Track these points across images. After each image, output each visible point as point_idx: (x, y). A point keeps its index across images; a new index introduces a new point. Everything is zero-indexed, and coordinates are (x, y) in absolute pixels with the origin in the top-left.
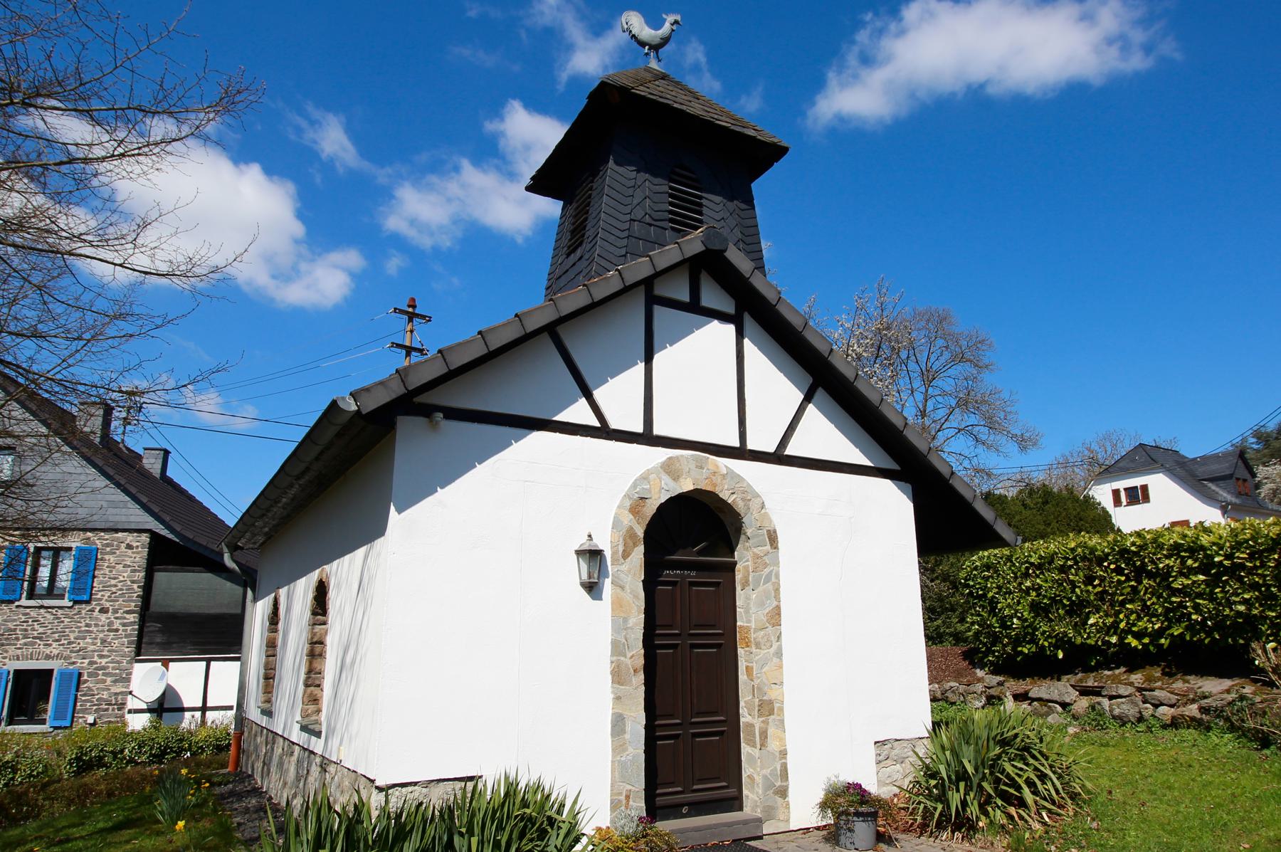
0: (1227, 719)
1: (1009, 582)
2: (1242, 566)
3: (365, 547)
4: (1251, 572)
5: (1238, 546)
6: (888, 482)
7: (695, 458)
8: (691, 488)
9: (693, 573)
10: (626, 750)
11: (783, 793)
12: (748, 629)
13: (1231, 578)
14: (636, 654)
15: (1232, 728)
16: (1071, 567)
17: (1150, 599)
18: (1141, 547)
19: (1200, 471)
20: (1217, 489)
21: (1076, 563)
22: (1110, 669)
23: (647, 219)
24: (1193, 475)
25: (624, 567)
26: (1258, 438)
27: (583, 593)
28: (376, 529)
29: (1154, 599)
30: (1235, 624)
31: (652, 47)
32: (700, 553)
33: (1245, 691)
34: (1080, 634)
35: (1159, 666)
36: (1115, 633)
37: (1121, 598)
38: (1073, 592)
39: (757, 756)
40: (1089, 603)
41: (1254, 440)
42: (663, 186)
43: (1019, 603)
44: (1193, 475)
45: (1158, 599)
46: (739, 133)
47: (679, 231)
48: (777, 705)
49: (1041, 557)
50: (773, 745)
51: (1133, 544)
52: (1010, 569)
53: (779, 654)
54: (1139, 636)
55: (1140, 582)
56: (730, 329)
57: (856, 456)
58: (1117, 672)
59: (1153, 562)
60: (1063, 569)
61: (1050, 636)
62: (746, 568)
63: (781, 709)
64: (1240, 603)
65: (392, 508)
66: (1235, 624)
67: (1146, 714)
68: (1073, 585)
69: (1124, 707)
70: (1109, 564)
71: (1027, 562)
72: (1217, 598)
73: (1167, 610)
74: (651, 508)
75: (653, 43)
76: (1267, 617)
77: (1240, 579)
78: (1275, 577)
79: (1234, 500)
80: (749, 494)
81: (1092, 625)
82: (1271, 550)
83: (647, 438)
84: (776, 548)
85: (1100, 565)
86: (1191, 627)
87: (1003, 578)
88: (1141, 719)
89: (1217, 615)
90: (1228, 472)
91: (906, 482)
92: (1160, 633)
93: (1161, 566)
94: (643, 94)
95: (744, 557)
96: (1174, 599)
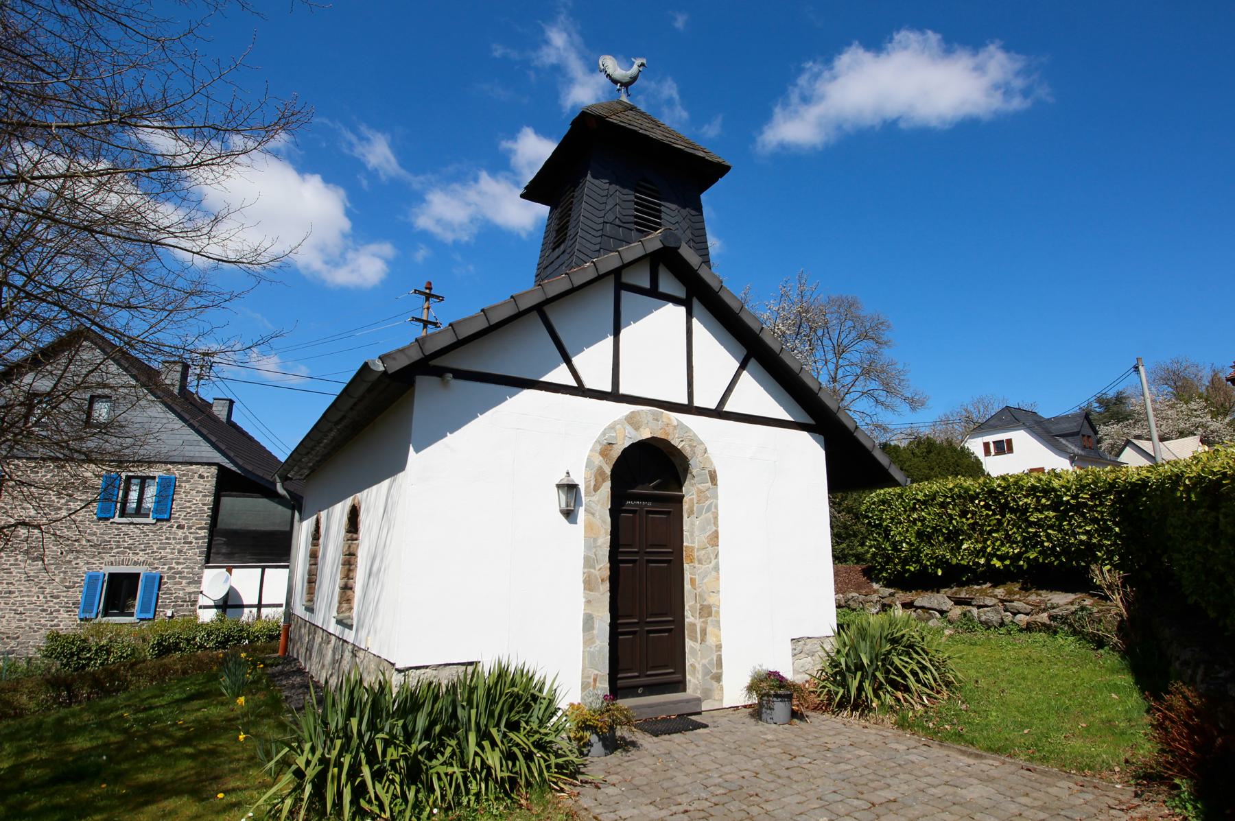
0: (1071, 625)
1: (900, 515)
2: (1085, 505)
4: (1091, 509)
5: (1082, 488)
6: (805, 433)
8: (649, 436)
9: (650, 504)
11: (718, 678)
12: (692, 549)
13: (1076, 513)
15: (1075, 632)
16: (950, 503)
17: (1011, 529)
18: (1005, 488)
19: (1054, 429)
20: (1067, 443)
21: (954, 500)
22: (978, 585)
24: (1048, 432)
25: (595, 498)
26: (1100, 403)
28: (398, 466)
29: (1015, 530)
33: (1085, 603)
34: (955, 556)
35: (1018, 582)
36: (983, 556)
37: (988, 528)
38: (951, 523)
40: (963, 532)
41: (1097, 405)
42: (630, 196)
44: (1048, 432)
45: (1018, 529)
48: (714, 609)
49: (925, 495)
50: (711, 640)
51: (999, 485)
52: (901, 504)
53: (717, 568)
54: (1001, 558)
55: (1004, 516)
56: (682, 310)
58: (984, 586)
59: (1014, 500)
60: (943, 505)
63: (718, 612)
64: (1082, 534)
65: (411, 449)
67: (1007, 620)
70: (979, 502)
71: (914, 499)
73: (1025, 539)
74: (617, 452)
75: (624, 81)
77: (1083, 515)
78: (1110, 514)
79: (1080, 452)
80: (695, 441)
81: (965, 550)
83: (614, 396)
85: (972, 502)
86: (1043, 552)
87: (895, 511)
88: (1002, 624)
89: (1065, 543)
91: (820, 433)
93: (1021, 503)
95: (690, 491)
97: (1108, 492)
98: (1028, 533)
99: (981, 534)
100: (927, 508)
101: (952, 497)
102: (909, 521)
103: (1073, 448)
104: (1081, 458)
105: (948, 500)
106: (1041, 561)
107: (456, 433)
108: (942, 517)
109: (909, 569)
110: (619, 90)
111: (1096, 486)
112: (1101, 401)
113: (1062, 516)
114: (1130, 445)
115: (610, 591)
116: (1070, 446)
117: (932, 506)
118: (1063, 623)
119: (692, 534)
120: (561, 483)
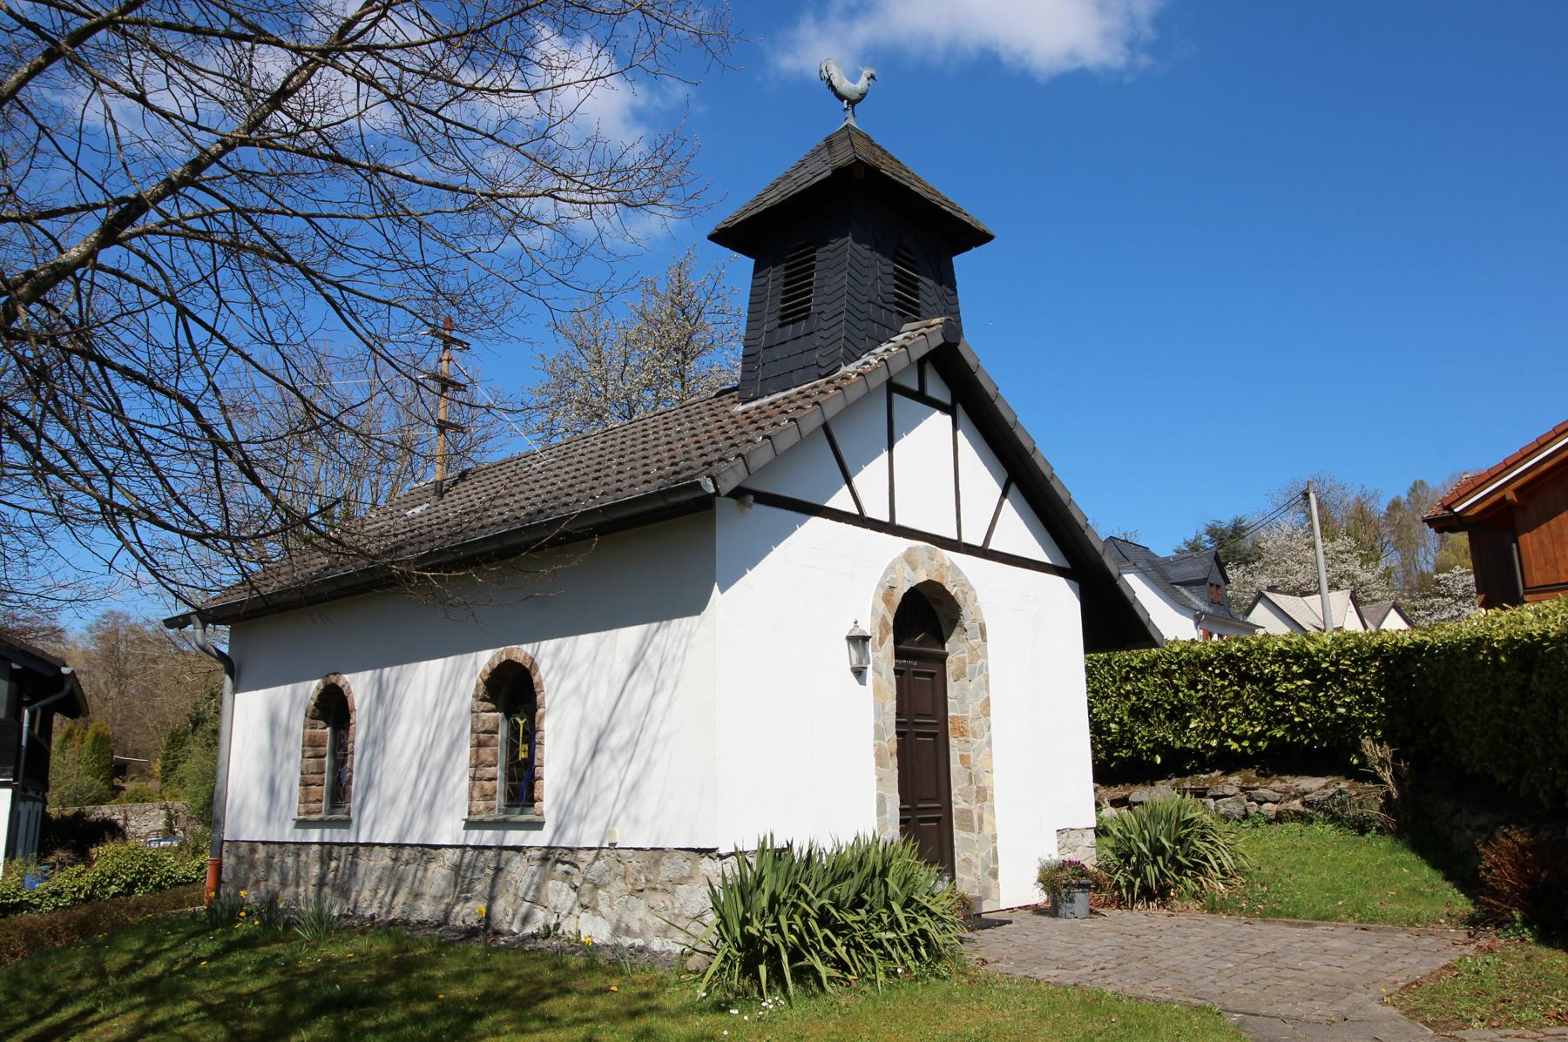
0: (1327, 812)
1: (1106, 686)
2: (1346, 672)
3: (645, 627)
4: (1353, 677)
8: (925, 579)
9: (915, 663)
12: (964, 720)
13: (1334, 683)
14: (891, 740)
16: (1175, 671)
18: (1248, 653)
19: (1175, 573)
20: (1190, 596)
21: (1180, 667)
23: (879, 301)
24: (1165, 578)
26: (1212, 536)
28: (696, 605)
29: (1256, 704)
31: (852, 103)
32: (920, 643)
34: (1180, 739)
36: (1215, 737)
40: (1191, 707)
41: (1207, 538)
42: (889, 266)
43: (1116, 707)
44: (1165, 578)
45: (1260, 703)
47: (904, 315)
49: (1143, 661)
50: (987, 830)
51: (1239, 650)
53: (989, 743)
54: (1238, 739)
55: (1243, 687)
56: (948, 419)
58: (1213, 775)
59: (1257, 667)
60: (1167, 674)
61: (1148, 741)
62: (962, 660)
63: (992, 796)
64: (1341, 706)
66: (1335, 724)
67: (1252, 811)
68: (1177, 689)
71: (1128, 666)
73: (1269, 714)
74: (897, 598)
76: (1365, 718)
77: (1343, 685)
78: (1375, 683)
79: (1207, 609)
80: (967, 587)
81: (1192, 729)
83: (891, 528)
84: (985, 641)
85: (1205, 670)
86: (1293, 730)
87: (1100, 682)
88: (1246, 816)
89: (1319, 718)
92: (1260, 735)
94: (917, 190)
95: (956, 648)
97: (1373, 658)
98: (1273, 706)
99: (1214, 709)
100: (1144, 677)
101: (1179, 663)
102: (1119, 695)
105: (1174, 667)
108: (1164, 689)
110: (846, 109)
112: (1213, 532)
113: (1319, 686)
116: (1193, 599)
117: (1152, 674)
118: (1320, 809)
119: (962, 701)
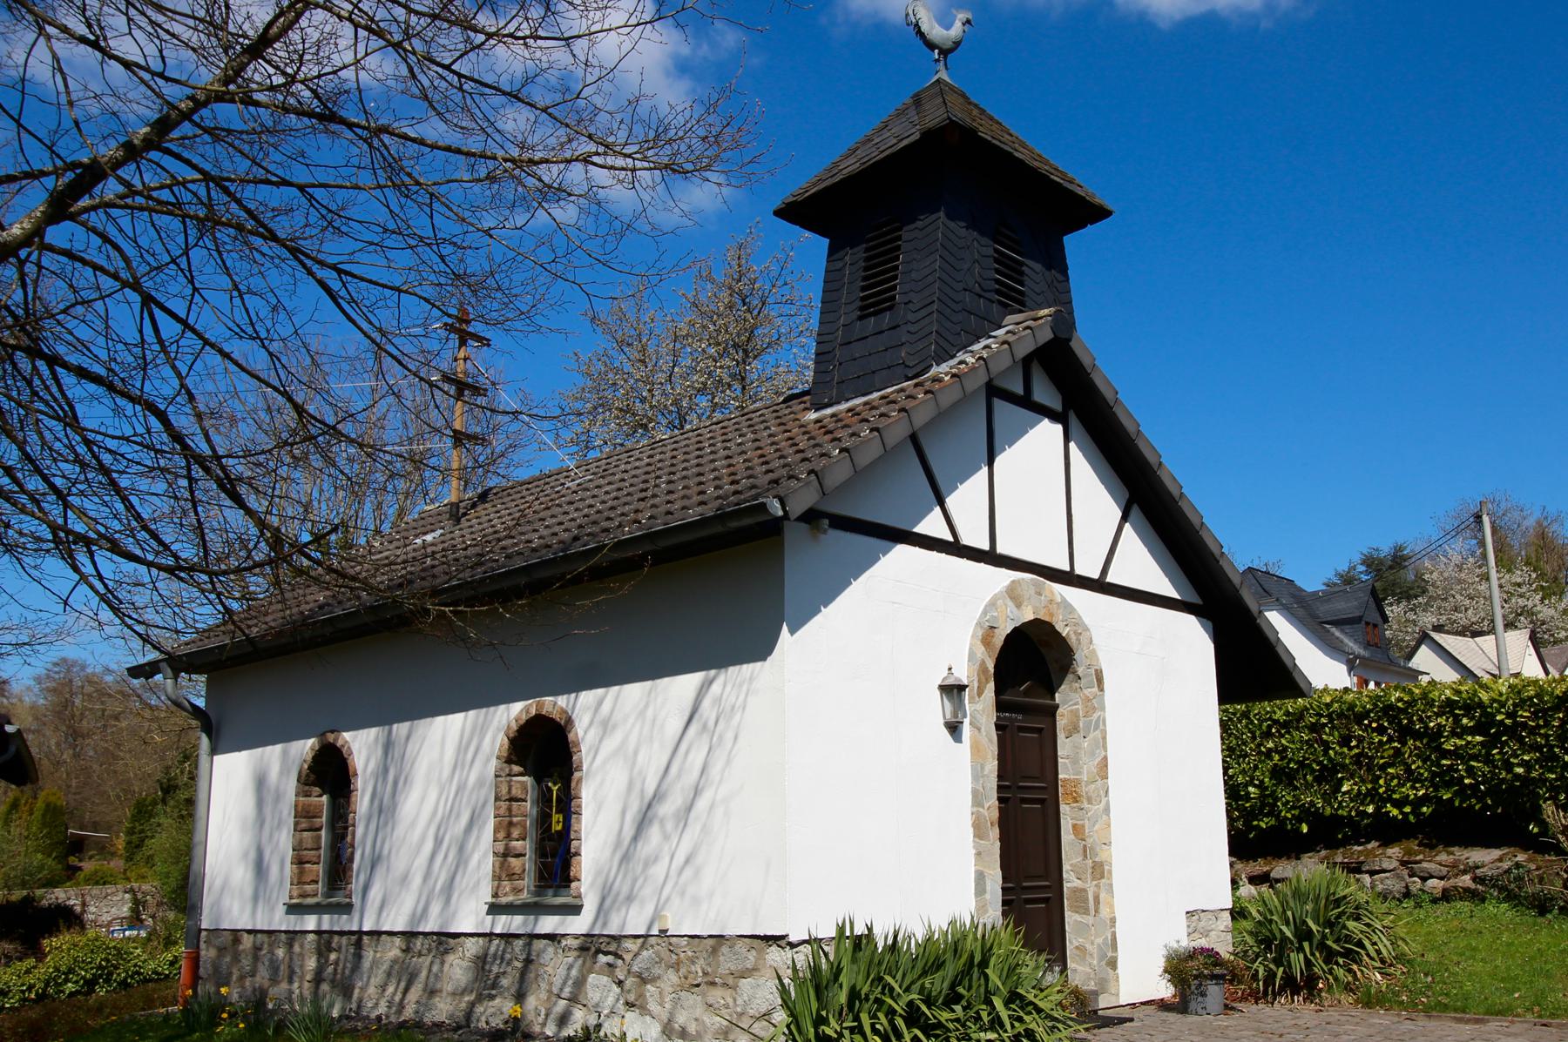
0: (1501, 889)
1: (1245, 743)
2: (1524, 726)
4: (1533, 731)
5: (1522, 703)
6: (1192, 618)
7: (1035, 584)
9: (1020, 717)
10: (986, 911)
11: (1113, 964)
13: (1510, 738)
15: (1508, 899)
16: (1325, 725)
17: (1414, 762)
18: (1409, 704)
19: (1323, 610)
21: (1331, 720)
22: (1360, 845)
24: (1313, 616)
25: (979, 707)
27: (945, 732)
28: (761, 648)
30: (1511, 787)
31: (945, 53)
32: (1026, 693)
33: (1518, 859)
35: (1417, 838)
36: (1372, 802)
37: (1382, 761)
38: (1326, 753)
39: (1090, 923)
40: (1344, 767)
41: (1363, 568)
43: (1256, 767)
44: (1313, 616)
45: (1424, 762)
46: (1072, 191)
48: (1106, 868)
49: (1287, 713)
50: (1104, 912)
51: (1400, 700)
52: (1247, 726)
53: (1107, 810)
54: (1399, 804)
55: (1404, 743)
57: (1167, 589)
58: (1369, 846)
59: (1421, 720)
60: (1315, 728)
61: (1293, 808)
62: (1075, 713)
63: (1110, 872)
64: (1518, 765)
65: (785, 628)
69: (1388, 882)
70: (1370, 723)
71: (1270, 719)
72: (1494, 761)
73: (1434, 775)
74: (999, 640)
75: (944, 47)
77: (1521, 740)
78: (1558, 738)
81: (1344, 793)
82: (1556, 709)
83: (991, 557)
85: (1360, 723)
86: (1463, 792)
87: (1237, 738)
88: (1407, 894)
89: (1492, 779)
90: (1357, 614)
91: (1208, 619)
93: (1432, 724)
95: (1067, 700)
96: (1444, 762)
99: (1370, 769)
101: (1329, 716)
103: (1351, 644)
104: (1365, 663)
105: (1324, 720)
106: (1457, 804)
107: (832, 606)
108: (1312, 746)
109: (1258, 826)
110: (938, 61)
111: (1541, 700)
112: (1370, 562)
114: (1427, 641)
115: (1001, 840)
116: (1346, 641)
117: (1297, 729)
120: (946, 683)
